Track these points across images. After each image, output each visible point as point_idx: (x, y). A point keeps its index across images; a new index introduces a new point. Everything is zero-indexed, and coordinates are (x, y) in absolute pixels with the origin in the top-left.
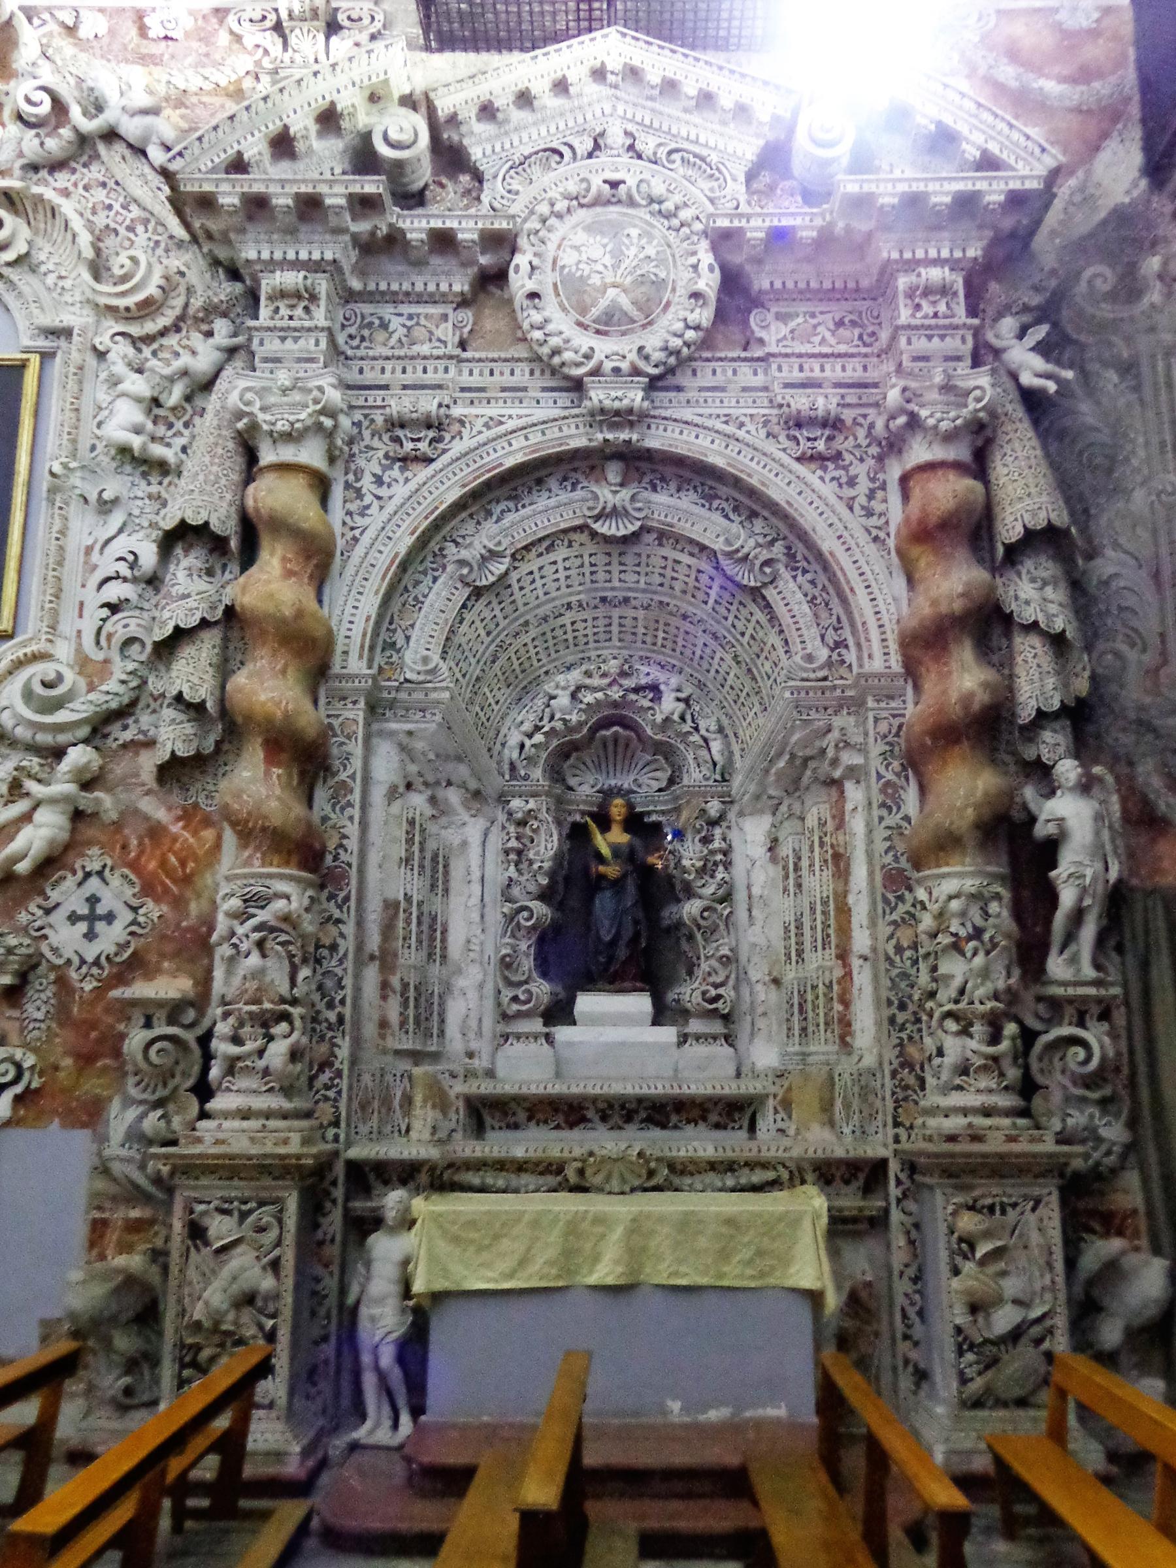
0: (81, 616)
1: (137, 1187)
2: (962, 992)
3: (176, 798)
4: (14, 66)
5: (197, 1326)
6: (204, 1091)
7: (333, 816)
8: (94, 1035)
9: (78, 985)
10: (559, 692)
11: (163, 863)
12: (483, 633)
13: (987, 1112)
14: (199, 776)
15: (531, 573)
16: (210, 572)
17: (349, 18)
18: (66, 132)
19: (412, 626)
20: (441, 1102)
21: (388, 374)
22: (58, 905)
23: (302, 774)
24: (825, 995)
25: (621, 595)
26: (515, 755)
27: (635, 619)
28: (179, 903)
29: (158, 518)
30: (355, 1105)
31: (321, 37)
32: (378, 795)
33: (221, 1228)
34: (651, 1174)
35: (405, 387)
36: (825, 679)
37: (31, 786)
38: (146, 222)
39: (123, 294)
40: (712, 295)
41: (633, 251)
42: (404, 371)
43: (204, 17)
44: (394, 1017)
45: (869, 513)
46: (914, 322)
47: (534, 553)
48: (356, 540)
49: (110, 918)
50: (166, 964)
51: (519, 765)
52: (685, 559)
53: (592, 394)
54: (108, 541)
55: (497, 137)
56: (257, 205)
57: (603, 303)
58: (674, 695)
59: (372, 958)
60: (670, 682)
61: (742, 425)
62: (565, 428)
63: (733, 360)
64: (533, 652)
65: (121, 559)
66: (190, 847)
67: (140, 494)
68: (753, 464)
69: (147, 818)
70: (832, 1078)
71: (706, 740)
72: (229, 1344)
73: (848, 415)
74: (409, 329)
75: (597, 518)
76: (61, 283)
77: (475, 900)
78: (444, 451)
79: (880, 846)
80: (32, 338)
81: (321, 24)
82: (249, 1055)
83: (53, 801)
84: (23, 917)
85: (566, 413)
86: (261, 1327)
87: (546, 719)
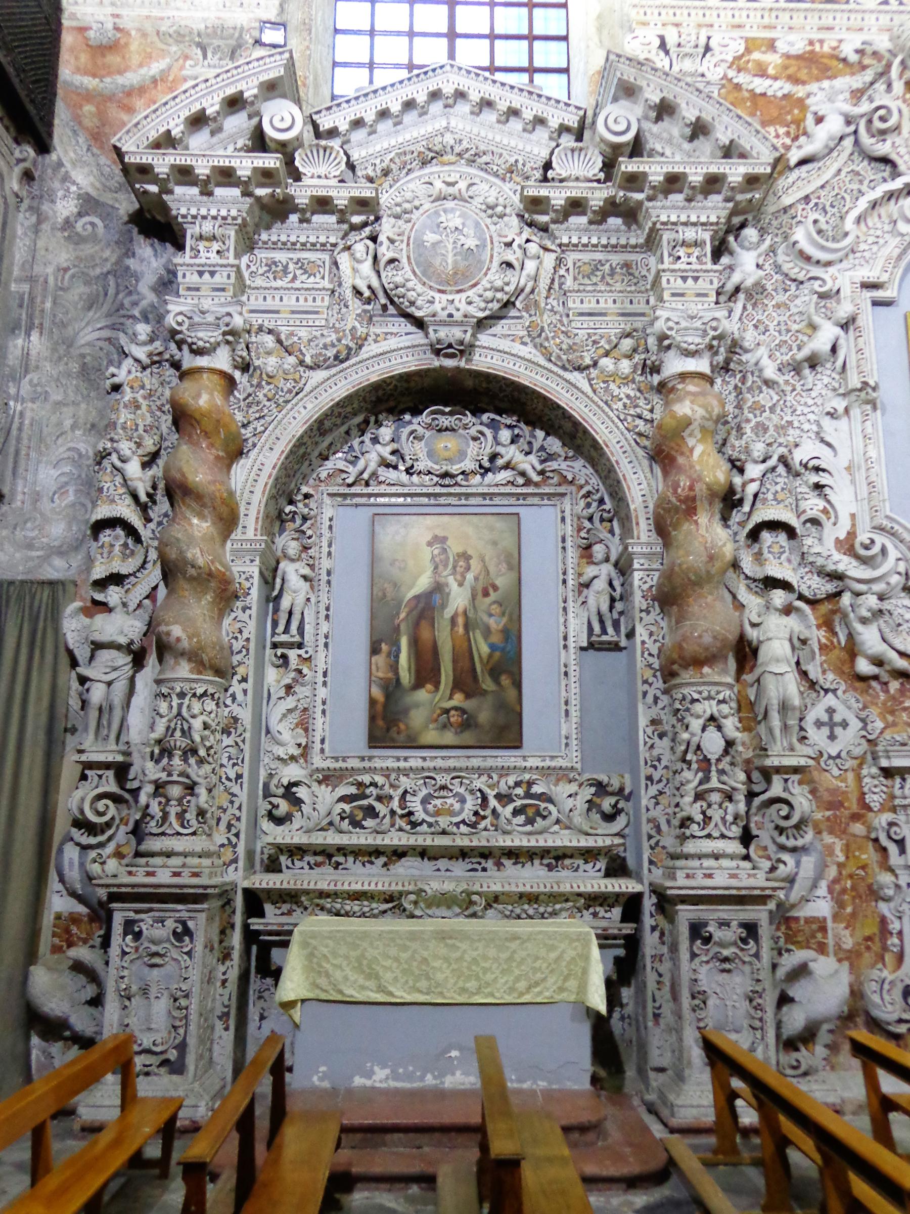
21: (602, 304)
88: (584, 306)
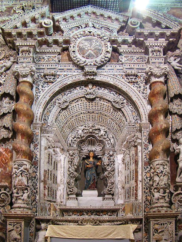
2: (158, 184)
6: (11, 204)
7: (34, 151)
10: (79, 130)
15: (74, 106)
19: (49, 116)
20: (55, 210)
21: (44, 67)
23: (28, 141)
24: (132, 189)
25: (92, 111)
26: (70, 142)
27: (95, 116)
28: (5, 168)
30: (40, 209)
32: (43, 148)
34: (96, 223)
35: (48, 69)
36: (134, 126)
40: (111, 52)
41: (94, 44)
44: (47, 194)
45: (143, 93)
46: (152, 56)
47: (74, 102)
48: (38, 98)
51: (71, 144)
52: (105, 103)
53: (86, 69)
56: (20, 35)
57: (88, 53)
58: (103, 131)
59: (42, 181)
60: (102, 128)
61: (117, 76)
62: (80, 76)
63: (115, 64)
64: (74, 122)
66: (7, 157)
68: (119, 83)
70: (133, 205)
71: (110, 139)
73: (139, 74)
74: (48, 59)
75: (87, 95)
77: (62, 172)
78: (56, 81)
79: (144, 157)
82: (20, 196)
85: (79, 73)
87: (77, 135)
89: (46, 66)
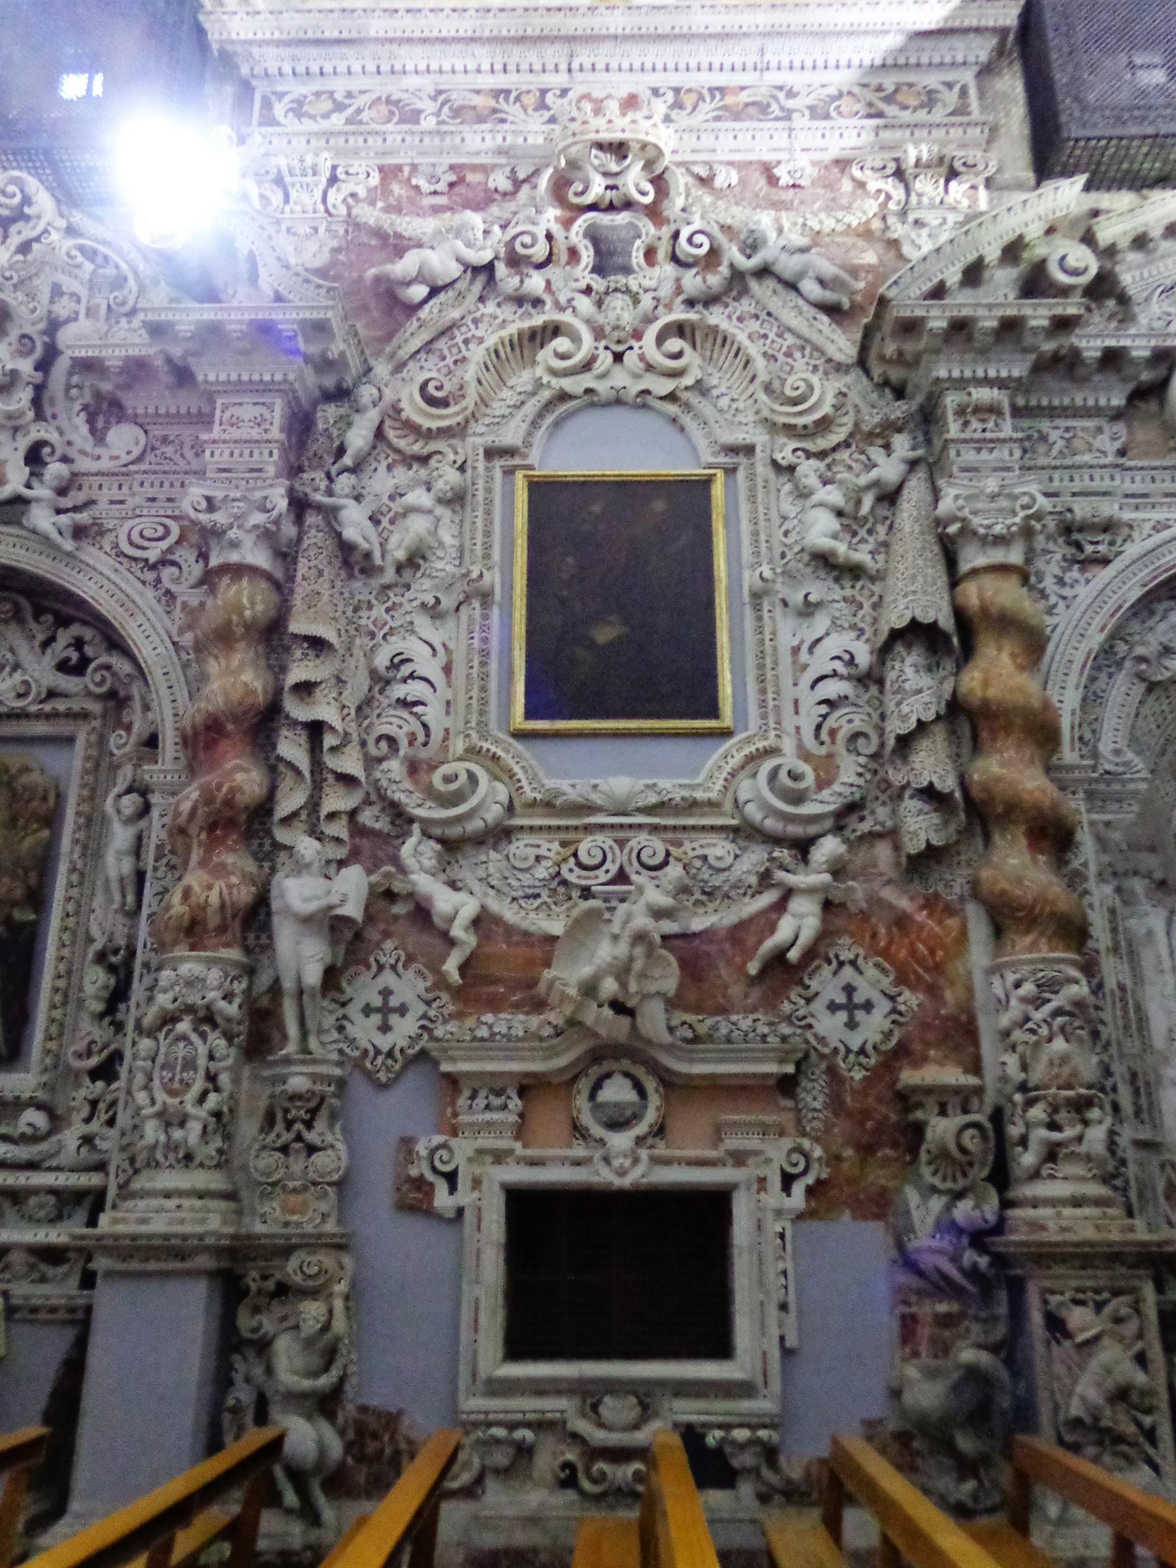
0: (797, 713)
1: (945, 1277)
3: (917, 887)
4: (665, 214)
5: (1077, 1423)
8: (870, 1124)
9: (846, 1074)
11: (913, 953)
12: (1153, 726)
13: (1077, 1202)
14: (935, 866)
16: (929, 669)
17: (347, 173)
18: (724, 270)
21: (1056, 483)
22: (817, 994)
28: (933, 991)
29: (856, 620)
31: (942, 181)
33: (1079, 1318)
35: (1074, 494)
37: (780, 875)
38: (803, 348)
39: (801, 413)
42: (1072, 480)
43: (826, 167)
46: (963, 436)
49: (868, 1006)
50: (932, 1052)
54: (819, 640)
55: (1146, 264)
65: (838, 658)
67: (837, 598)
69: (891, 907)
72: (1107, 1442)
76: (734, 406)
80: (714, 454)
81: (944, 170)
83: (810, 891)
84: (786, 1007)
86: (1139, 1424)
88: (1094, 484)
89: (1066, 483)
